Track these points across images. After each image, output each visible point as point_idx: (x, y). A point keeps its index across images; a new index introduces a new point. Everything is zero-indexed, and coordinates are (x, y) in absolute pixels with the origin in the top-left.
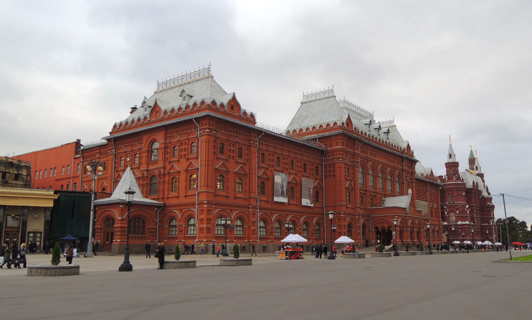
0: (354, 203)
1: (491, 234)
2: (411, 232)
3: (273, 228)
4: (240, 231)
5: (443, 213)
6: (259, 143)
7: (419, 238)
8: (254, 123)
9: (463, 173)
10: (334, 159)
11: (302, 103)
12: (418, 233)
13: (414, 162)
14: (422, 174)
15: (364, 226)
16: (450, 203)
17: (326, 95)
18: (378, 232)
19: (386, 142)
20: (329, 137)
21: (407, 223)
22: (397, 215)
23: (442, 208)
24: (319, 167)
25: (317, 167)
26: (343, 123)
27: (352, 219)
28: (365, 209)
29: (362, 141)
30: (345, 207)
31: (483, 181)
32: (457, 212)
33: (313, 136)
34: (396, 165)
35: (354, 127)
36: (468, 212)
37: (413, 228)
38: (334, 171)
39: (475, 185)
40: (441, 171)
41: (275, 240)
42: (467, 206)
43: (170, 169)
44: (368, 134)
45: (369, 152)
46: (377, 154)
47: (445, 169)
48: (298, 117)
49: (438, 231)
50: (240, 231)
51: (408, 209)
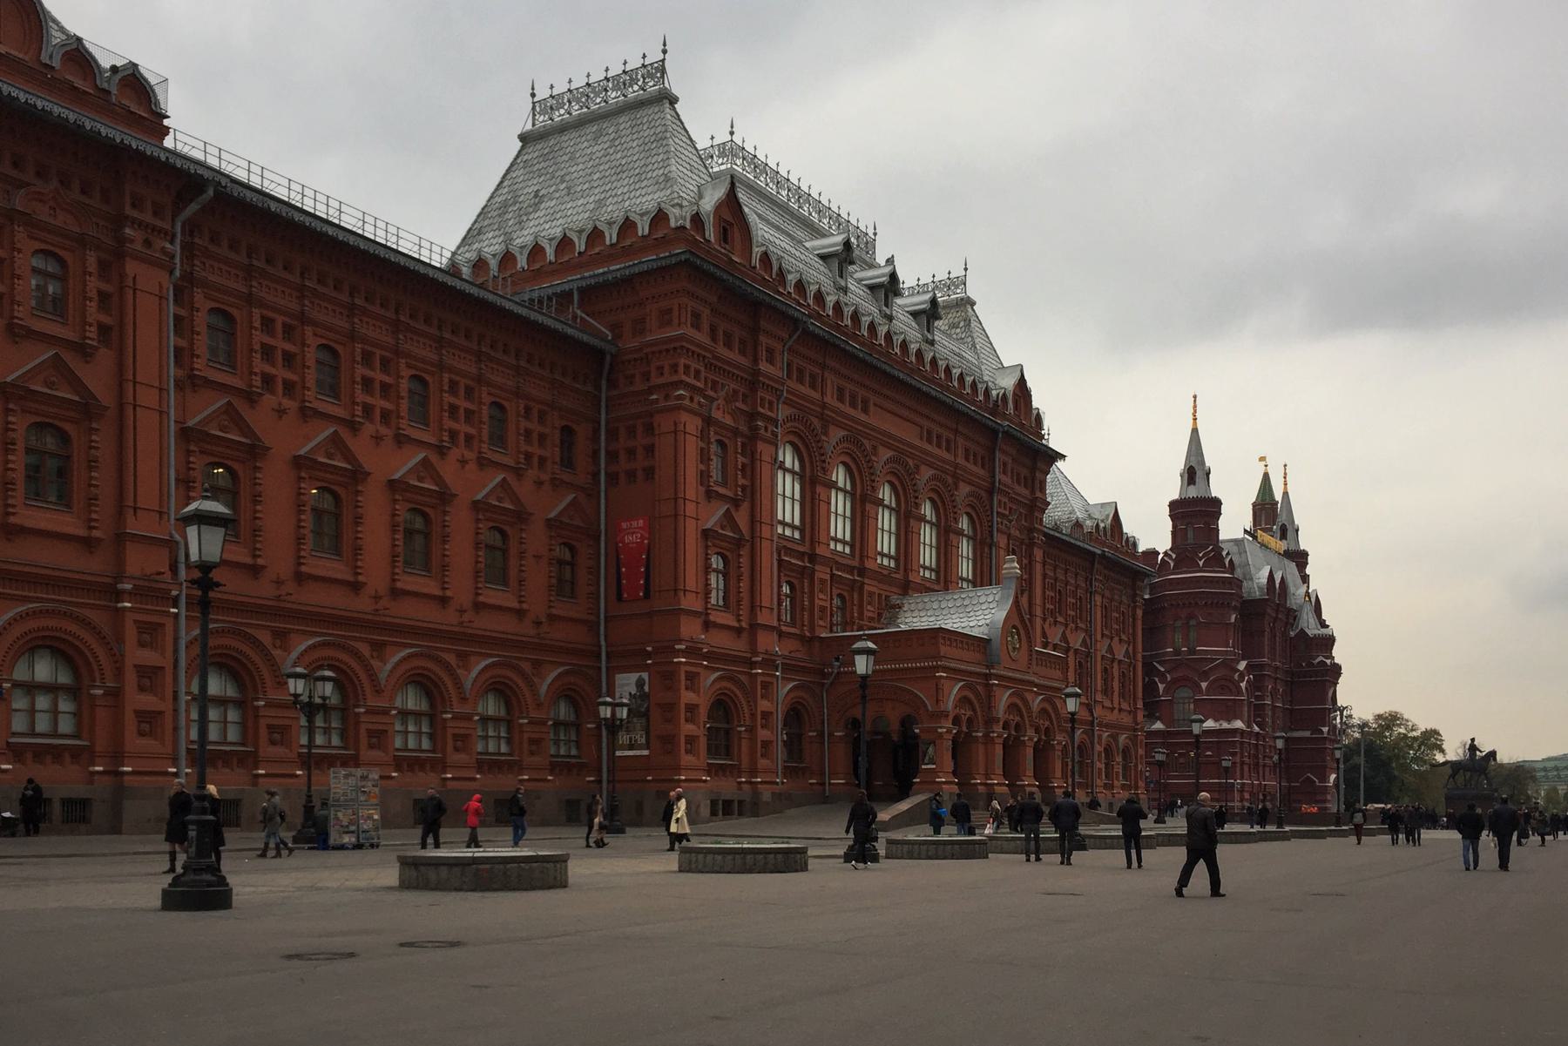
0: (745, 603)
1: (591, 814)
3: (544, 723)
4: (420, 733)
5: (1150, 688)
6: (188, 248)
7: (1042, 773)
8: (155, 123)
9: (1237, 542)
10: (650, 391)
11: (524, 138)
13: (1040, 458)
15: (795, 715)
16: (1177, 652)
17: (634, 92)
19: (919, 354)
20: (626, 283)
21: (989, 705)
22: (945, 669)
23: (1149, 669)
25: (567, 431)
26: (697, 219)
27: (731, 679)
28: (801, 638)
29: (795, 321)
30: (699, 622)
31: (1305, 579)
32: (1204, 685)
33: (559, 283)
34: (961, 461)
35: (757, 251)
36: (1243, 685)
37: (1017, 727)
38: (650, 450)
39: (1277, 590)
40: (1151, 531)
41: (479, 769)
42: (1242, 665)
44: (830, 300)
45: (831, 381)
47: (1168, 525)
48: (505, 205)
49: (1126, 752)
50: (420, 733)
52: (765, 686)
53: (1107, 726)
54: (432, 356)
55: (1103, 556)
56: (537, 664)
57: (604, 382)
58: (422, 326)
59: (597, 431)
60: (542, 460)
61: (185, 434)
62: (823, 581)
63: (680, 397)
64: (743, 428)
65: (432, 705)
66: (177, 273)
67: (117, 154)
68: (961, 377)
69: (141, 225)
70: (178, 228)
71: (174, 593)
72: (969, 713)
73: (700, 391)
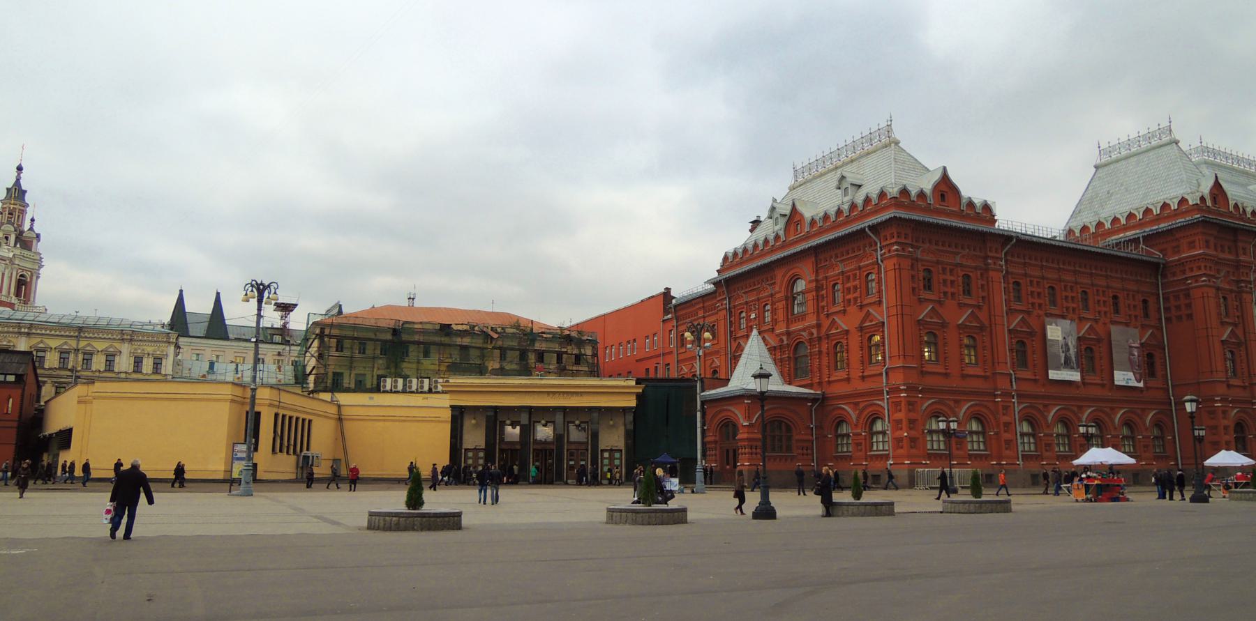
8: (993, 220)
10: (1187, 279)
25: (1145, 301)
26: (1202, 199)
35: (1232, 203)
38: (1189, 306)
43: (830, 328)
52: (1224, 412)
54: (1056, 276)
56: (1080, 408)
58: (1033, 262)
61: (1009, 331)
64: (1234, 288)
65: (983, 427)
67: (983, 235)
69: (993, 258)
73: (1213, 276)
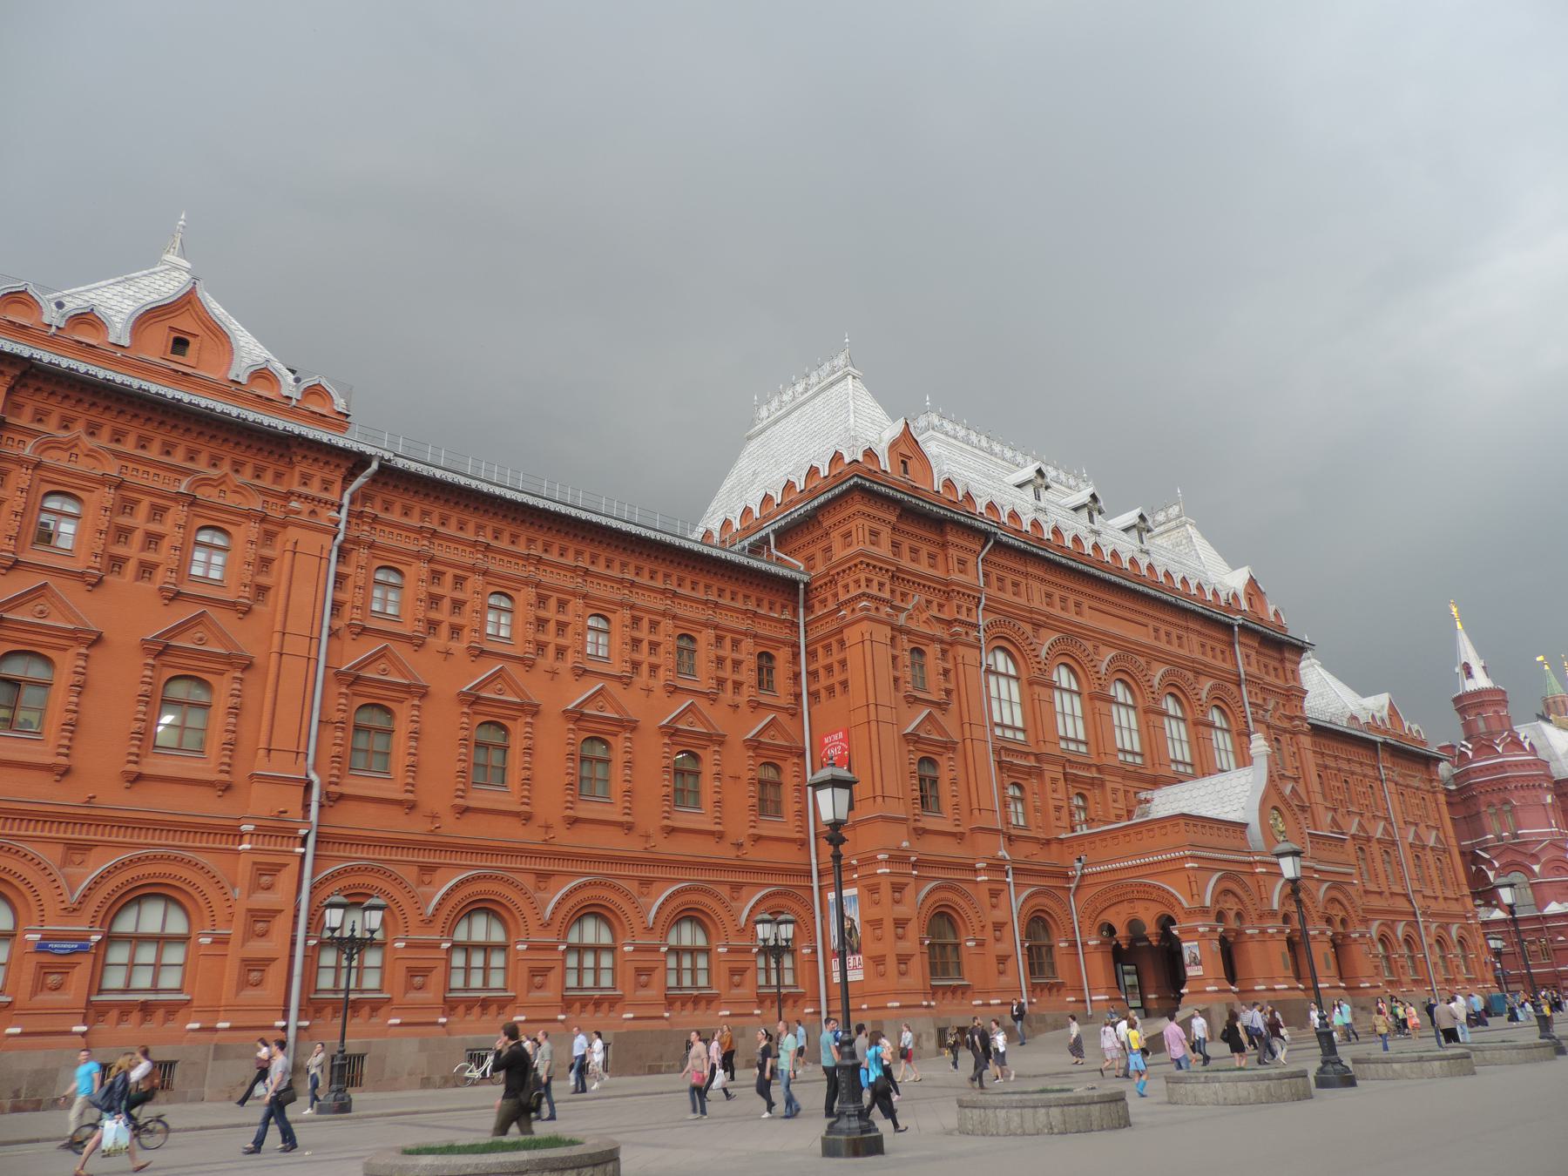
2: (1291, 943)
12: (1339, 945)
14: (1354, 718)
18: (1119, 956)
24: (782, 655)
25: (766, 658)
38: (843, 663)
46: (1086, 603)
49: (1462, 941)
51: (1255, 829)
52: (994, 894)
53: (1434, 915)
55: (1385, 744)
56: (736, 887)
57: (801, 611)
59: (796, 655)
60: (654, 668)
62: (1054, 780)
63: (866, 609)
65: (614, 938)
66: (340, 537)
68: (1184, 581)
70: (346, 500)
71: (303, 832)
72: (1342, 914)
